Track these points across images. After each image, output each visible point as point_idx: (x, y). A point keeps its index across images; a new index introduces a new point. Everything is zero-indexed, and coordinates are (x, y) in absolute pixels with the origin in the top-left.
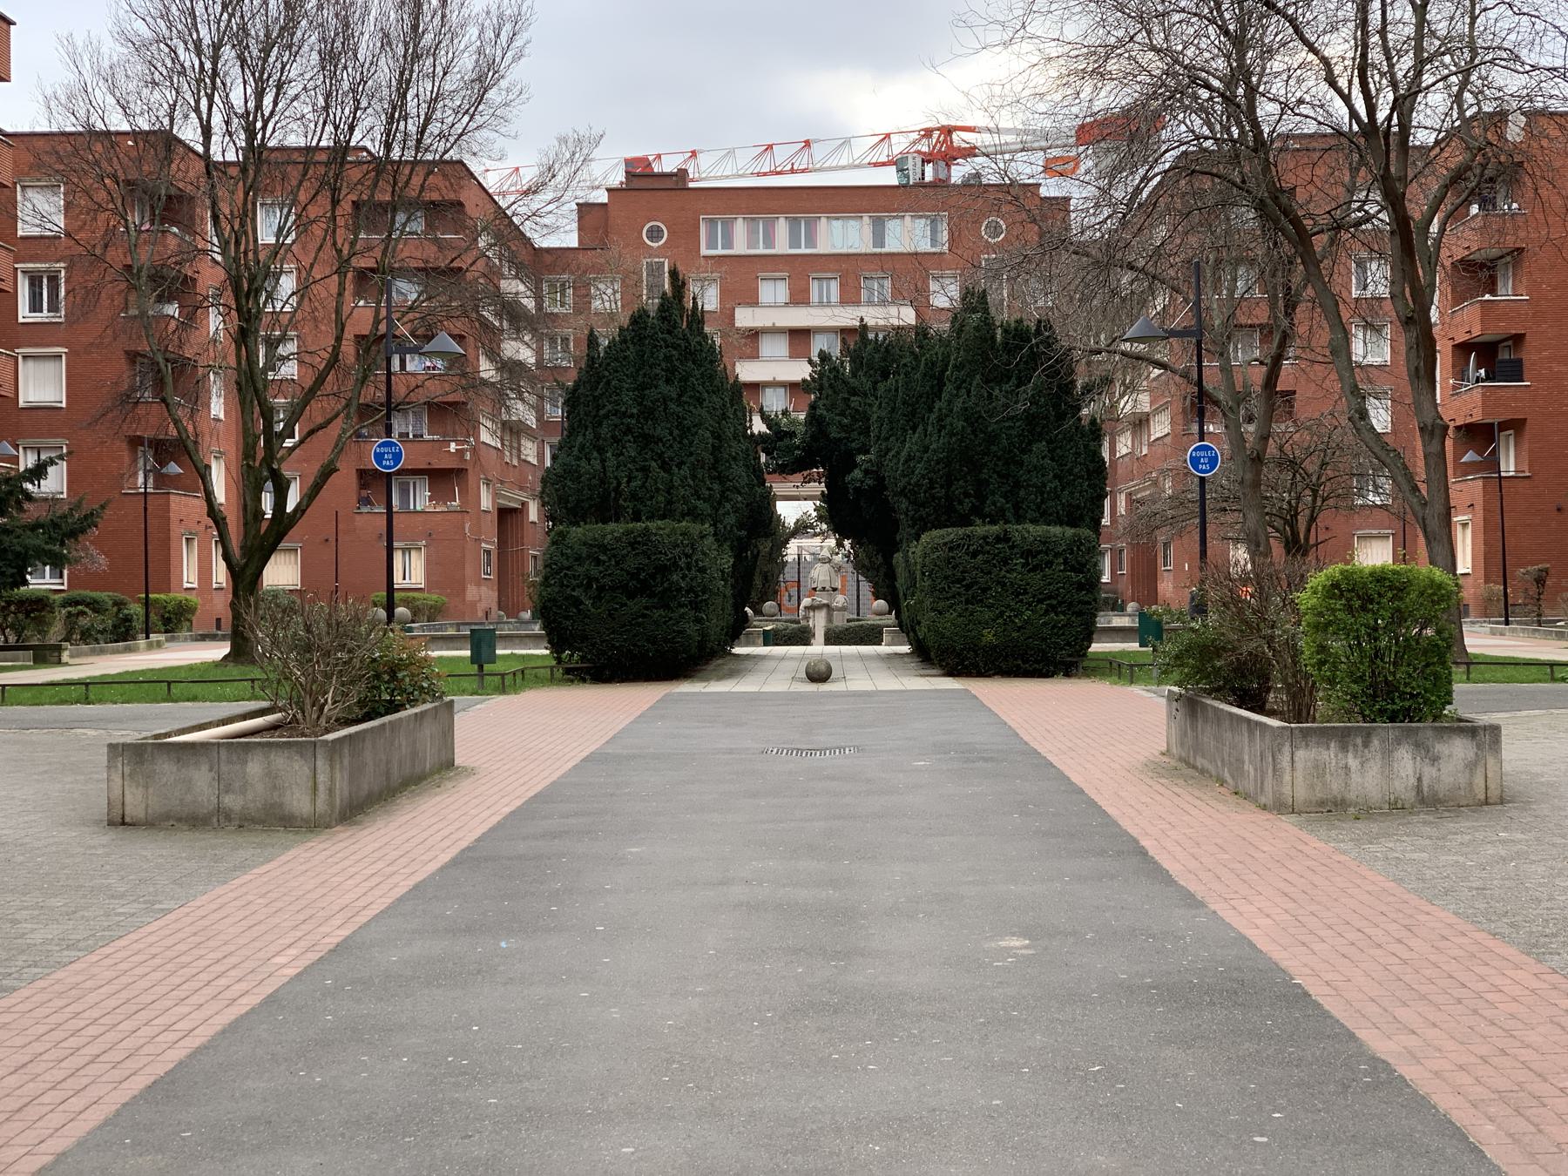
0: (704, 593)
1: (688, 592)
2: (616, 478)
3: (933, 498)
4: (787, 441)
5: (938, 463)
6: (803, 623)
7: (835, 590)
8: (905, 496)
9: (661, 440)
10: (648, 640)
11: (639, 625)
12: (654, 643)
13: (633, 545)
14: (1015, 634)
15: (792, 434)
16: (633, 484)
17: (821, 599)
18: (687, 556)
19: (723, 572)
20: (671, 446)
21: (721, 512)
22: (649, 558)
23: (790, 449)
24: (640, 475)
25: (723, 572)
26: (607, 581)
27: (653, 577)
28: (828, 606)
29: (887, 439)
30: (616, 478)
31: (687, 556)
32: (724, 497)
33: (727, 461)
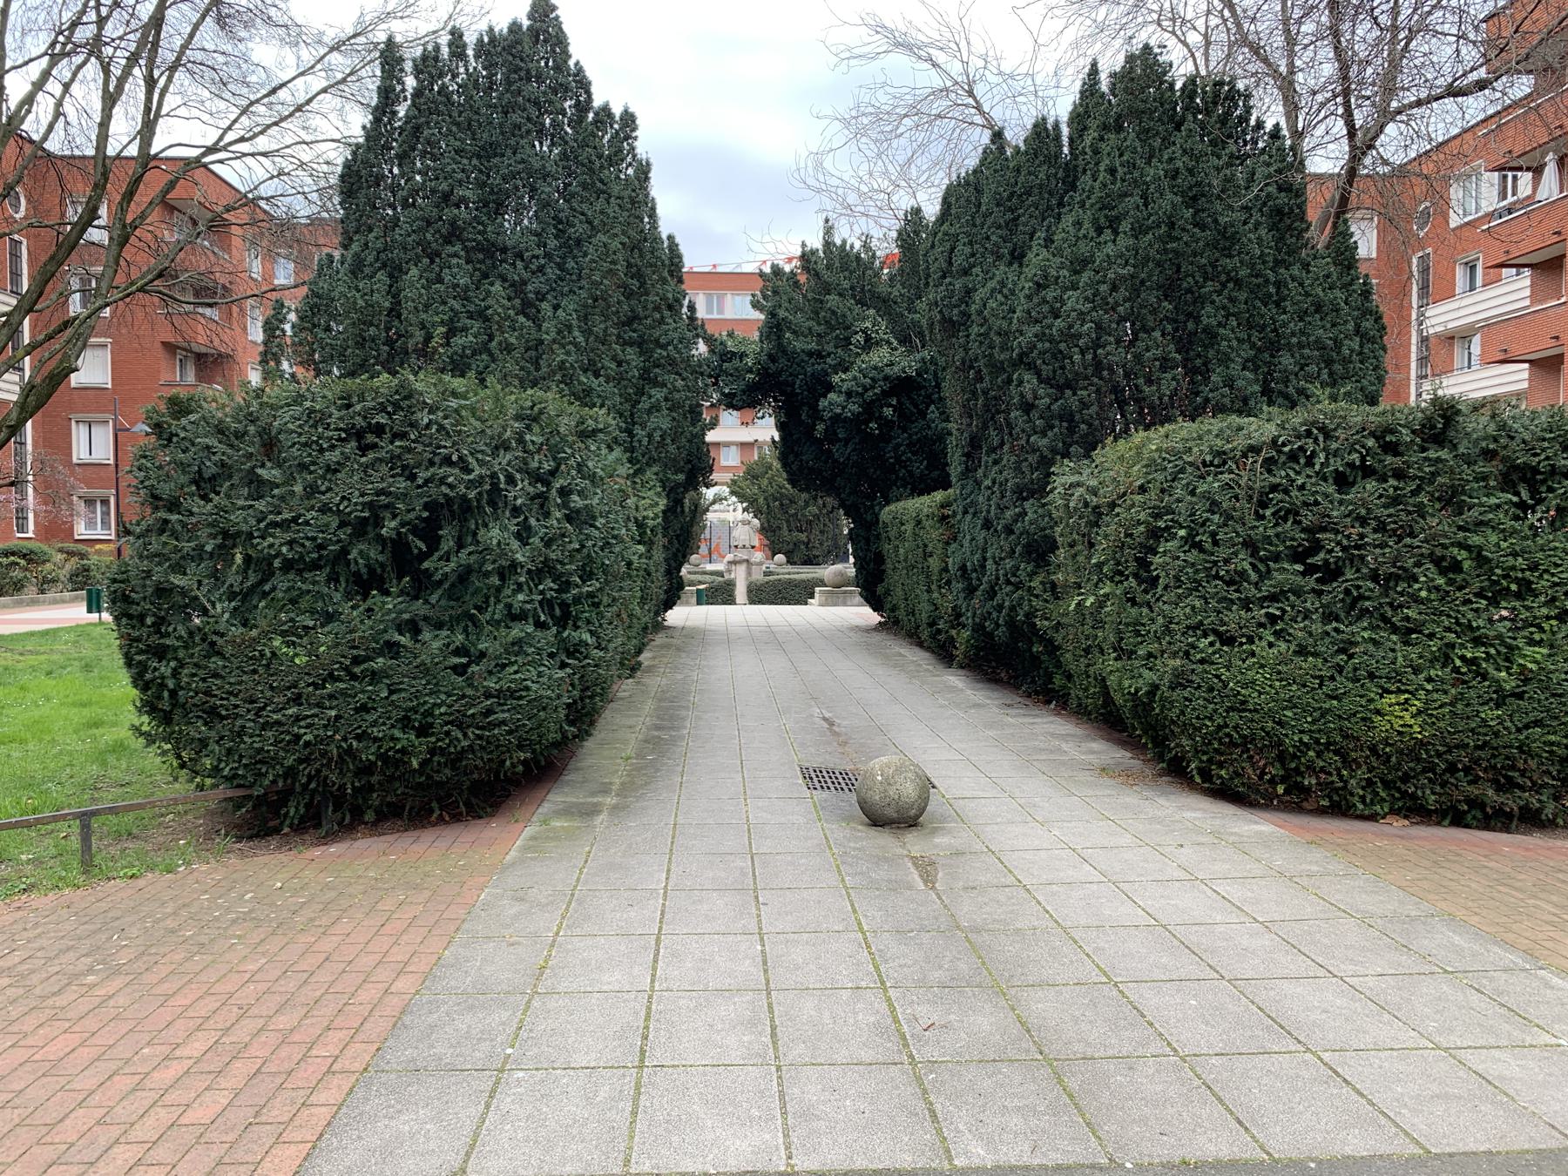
0: (587, 576)
1: (537, 575)
2: (423, 326)
3: (1098, 365)
4: (737, 363)
5: (1114, 288)
6: (727, 576)
7: (753, 547)
8: (1031, 367)
9: (520, 256)
10: (405, 722)
11: (375, 677)
12: (423, 731)
13: (362, 436)
14: (1490, 714)
15: (743, 355)
16: (459, 341)
17: (742, 555)
18: (536, 477)
19: (640, 525)
20: (541, 269)
21: (644, 404)
22: (412, 477)
23: (737, 375)
24: (476, 325)
25: (640, 525)
26: (276, 542)
27: (429, 531)
28: (747, 561)
29: (966, 272)
30: (423, 326)
31: (536, 477)
32: (648, 378)
33: (657, 308)
